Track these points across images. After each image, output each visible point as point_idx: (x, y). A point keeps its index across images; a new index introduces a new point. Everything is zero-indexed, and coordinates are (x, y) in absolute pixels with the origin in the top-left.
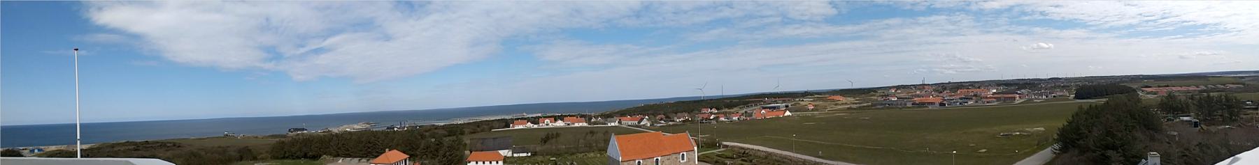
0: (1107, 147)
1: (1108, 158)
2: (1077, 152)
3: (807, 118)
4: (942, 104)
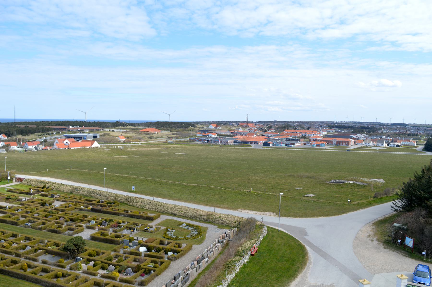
2: (424, 212)
3: (118, 151)
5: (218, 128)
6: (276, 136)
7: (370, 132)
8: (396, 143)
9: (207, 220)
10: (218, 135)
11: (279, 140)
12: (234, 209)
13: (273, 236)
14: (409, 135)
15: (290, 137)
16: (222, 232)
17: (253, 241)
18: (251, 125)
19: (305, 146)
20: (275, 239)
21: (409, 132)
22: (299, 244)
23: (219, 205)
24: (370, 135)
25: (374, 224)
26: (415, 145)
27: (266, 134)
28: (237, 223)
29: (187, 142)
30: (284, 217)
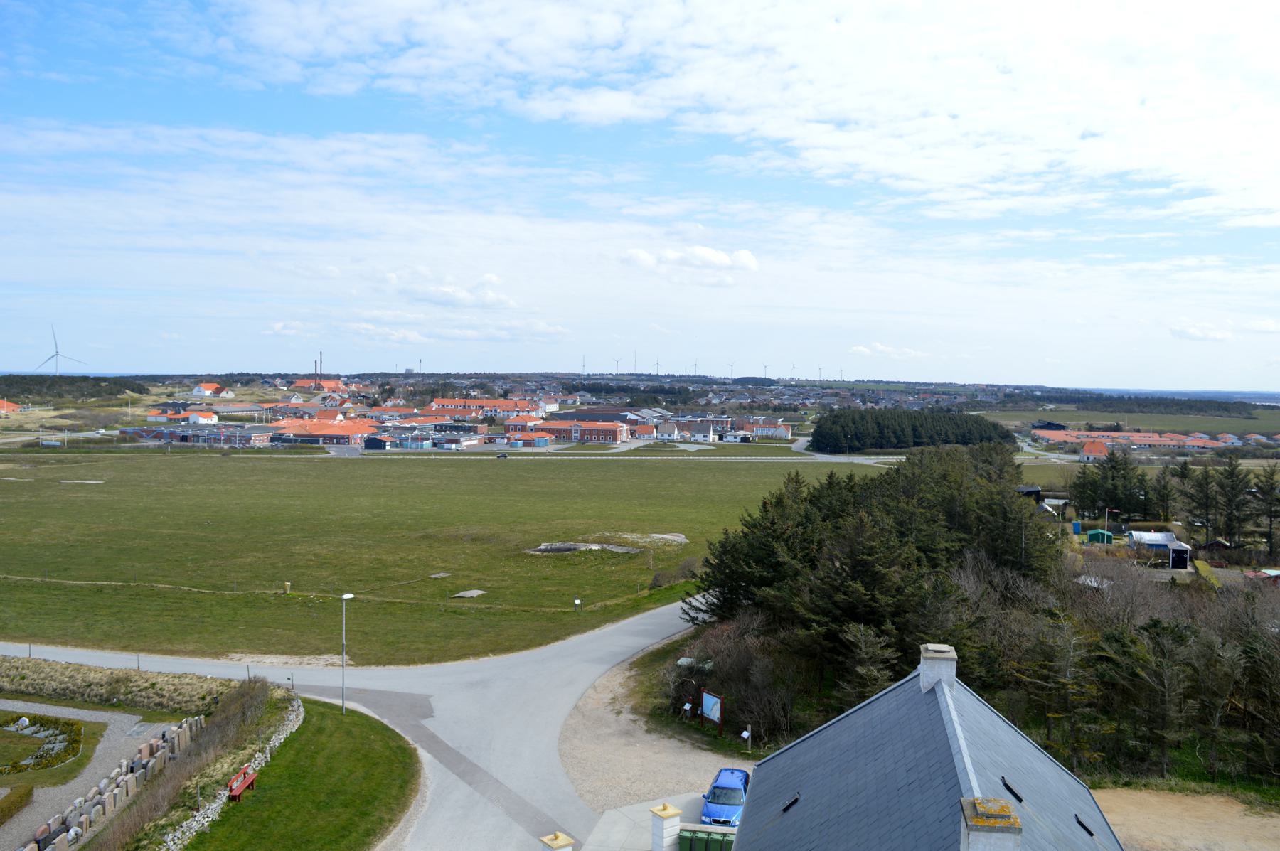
0: (854, 613)
1: (850, 647)
2: (758, 621)
4: (373, 443)
5: (223, 394)
6: (404, 417)
7: (674, 403)
8: (742, 433)
9: (108, 700)
10: (220, 418)
11: (413, 429)
12: (216, 655)
13: (320, 730)
14: (776, 409)
15: (448, 421)
16: (151, 734)
17: (243, 754)
18: (332, 384)
19: (490, 448)
20: (324, 738)
21: (776, 402)
22: (399, 747)
23: (169, 646)
24: (676, 412)
25: (634, 665)
26: (790, 437)
27: (376, 412)
28: (208, 699)
29: (110, 441)
30: (373, 667)
